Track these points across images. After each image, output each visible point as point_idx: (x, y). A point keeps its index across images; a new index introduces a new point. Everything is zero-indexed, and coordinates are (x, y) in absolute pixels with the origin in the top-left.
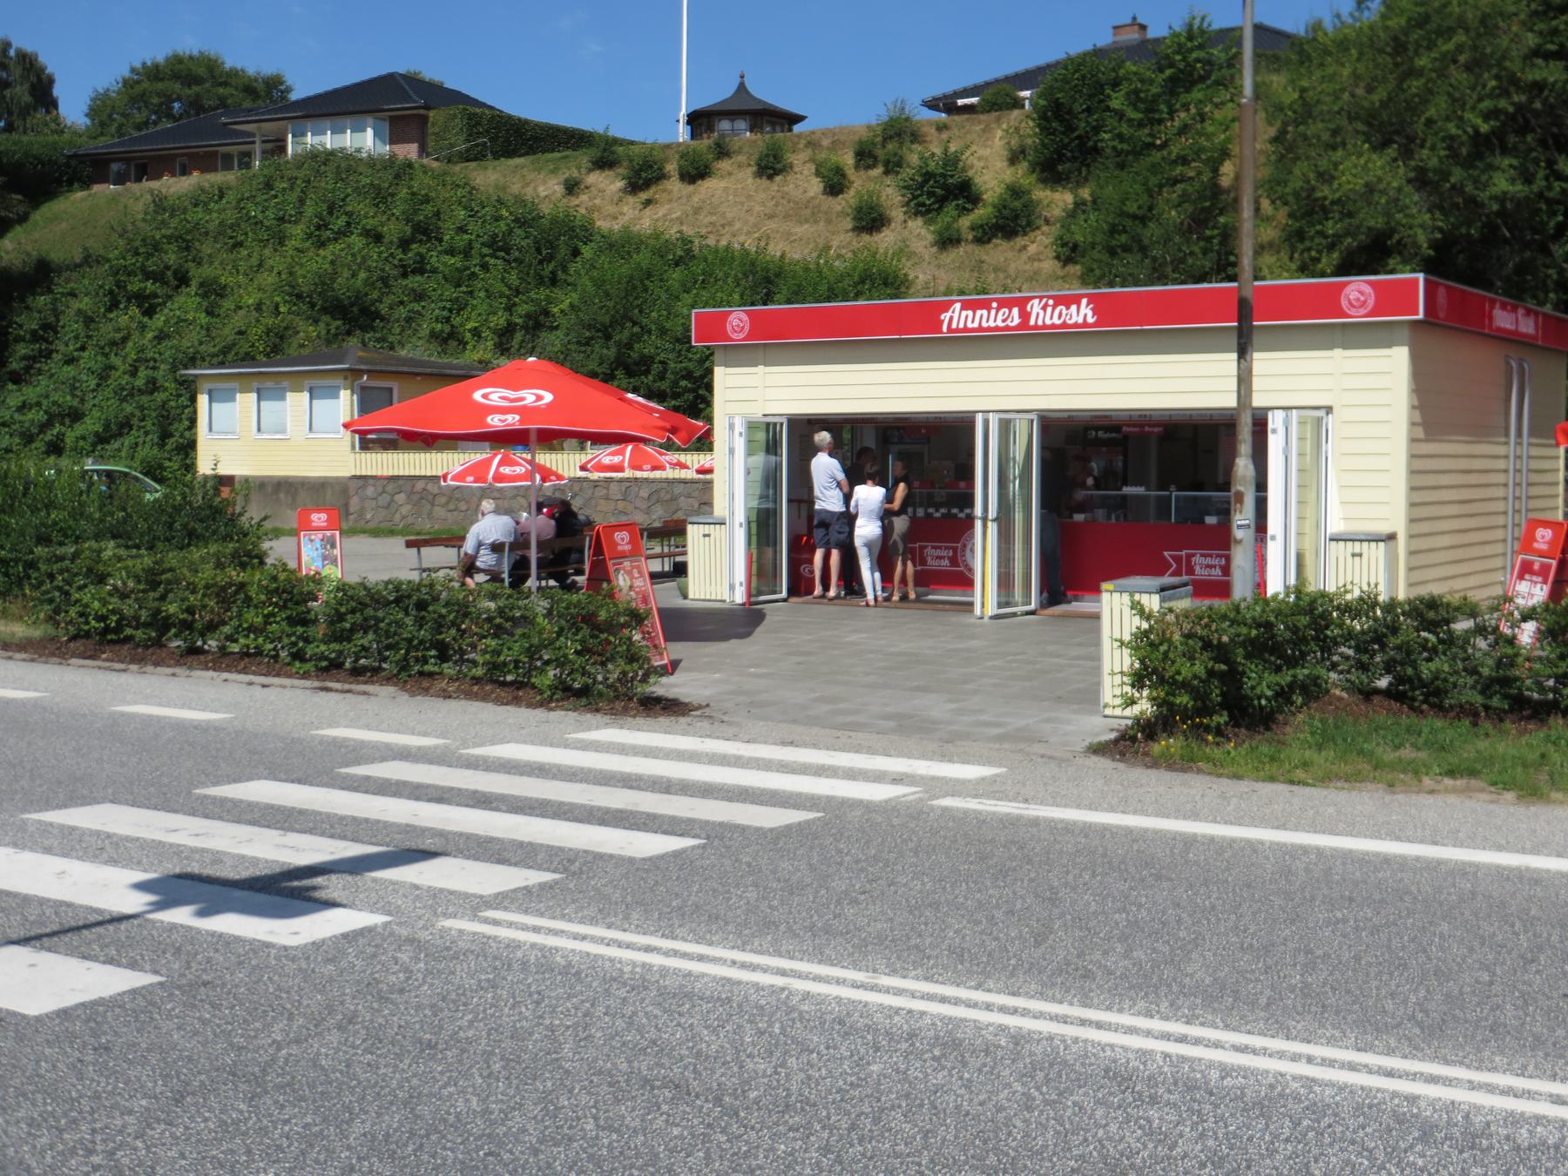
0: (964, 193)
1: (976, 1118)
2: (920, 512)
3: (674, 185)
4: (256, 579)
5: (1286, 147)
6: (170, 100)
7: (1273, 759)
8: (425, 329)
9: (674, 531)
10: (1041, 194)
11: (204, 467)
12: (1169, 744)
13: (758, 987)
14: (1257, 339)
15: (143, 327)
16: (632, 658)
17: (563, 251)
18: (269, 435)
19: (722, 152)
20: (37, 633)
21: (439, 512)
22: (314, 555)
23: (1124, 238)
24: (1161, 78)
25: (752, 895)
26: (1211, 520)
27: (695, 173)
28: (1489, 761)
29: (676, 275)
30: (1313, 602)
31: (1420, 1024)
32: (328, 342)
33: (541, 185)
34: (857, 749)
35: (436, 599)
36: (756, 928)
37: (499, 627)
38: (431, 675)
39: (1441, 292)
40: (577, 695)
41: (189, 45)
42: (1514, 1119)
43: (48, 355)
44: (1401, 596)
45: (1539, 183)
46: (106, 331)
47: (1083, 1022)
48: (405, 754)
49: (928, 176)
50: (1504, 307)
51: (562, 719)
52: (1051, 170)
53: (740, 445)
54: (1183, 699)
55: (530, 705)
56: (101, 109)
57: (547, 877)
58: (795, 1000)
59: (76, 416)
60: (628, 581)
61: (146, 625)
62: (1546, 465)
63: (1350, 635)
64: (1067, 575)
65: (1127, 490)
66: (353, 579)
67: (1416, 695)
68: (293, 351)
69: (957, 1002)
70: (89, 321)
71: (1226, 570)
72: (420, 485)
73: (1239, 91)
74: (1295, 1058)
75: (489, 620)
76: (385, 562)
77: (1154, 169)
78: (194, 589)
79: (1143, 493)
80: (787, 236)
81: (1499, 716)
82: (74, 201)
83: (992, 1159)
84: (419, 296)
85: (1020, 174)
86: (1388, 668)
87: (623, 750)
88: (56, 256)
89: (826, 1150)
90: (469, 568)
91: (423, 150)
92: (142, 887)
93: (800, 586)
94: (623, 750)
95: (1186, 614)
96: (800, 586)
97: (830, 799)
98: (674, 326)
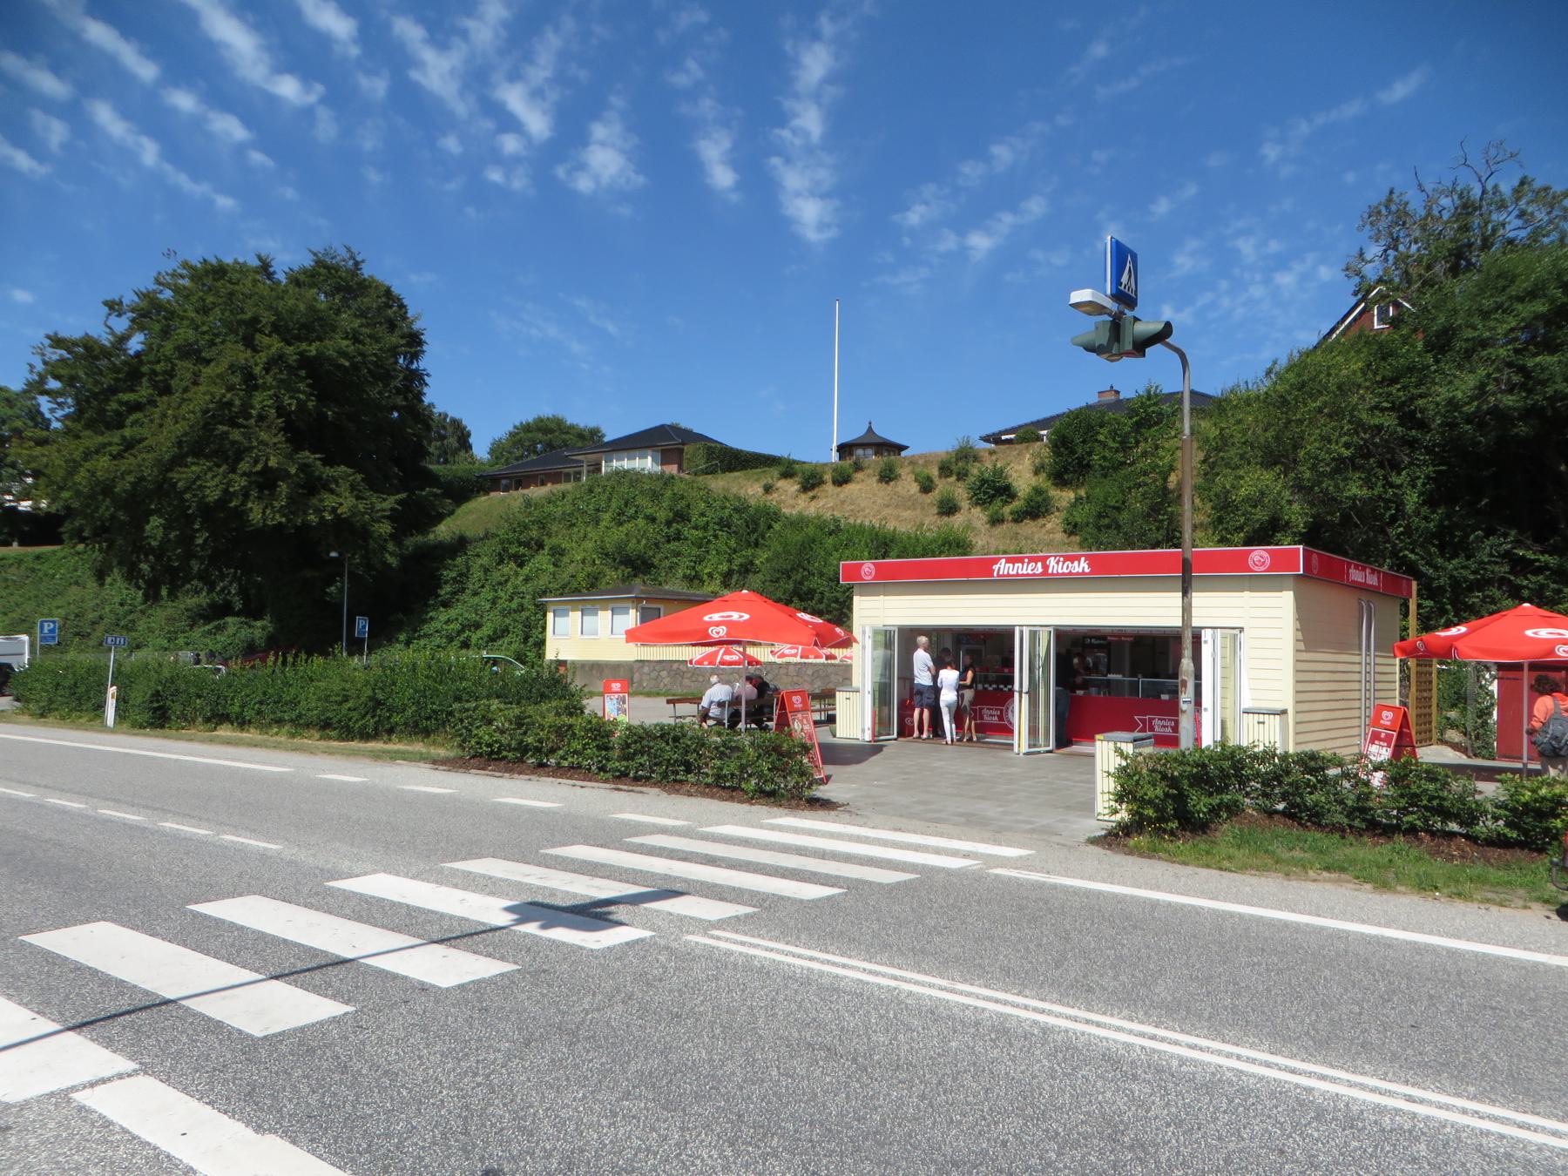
0: (1007, 492)
1: (1019, 1081)
2: (980, 687)
3: (829, 488)
4: (576, 722)
5: (1210, 468)
6: (534, 443)
7: (1208, 853)
8: (680, 573)
9: (828, 696)
10: (1054, 493)
11: (550, 655)
12: (1141, 840)
13: (880, 987)
14: (1194, 583)
15: (517, 574)
16: (802, 774)
17: (762, 526)
18: (585, 636)
19: (858, 467)
20: (452, 754)
21: (686, 682)
22: (616, 710)
23: (1107, 521)
24: (1130, 422)
25: (876, 926)
26: (1165, 697)
27: (842, 480)
28: (1353, 862)
29: (830, 541)
30: (1233, 753)
31: (1313, 1038)
32: (623, 581)
33: (749, 488)
34: (941, 835)
35: (684, 736)
36: (878, 948)
37: (722, 753)
38: (681, 782)
39: (1315, 556)
40: (768, 796)
41: (547, 411)
42: (1380, 1110)
43: (463, 590)
44: (1291, 751)
45: (1378, 490)
46: (496, 576)
47: (1088, 1022)
48: (664, 831)
49: (984, 481)
50: (1356, 567)
51: (760, 811)
52: (1060, 478)
53: (869, 643)
54: (1150, 812)
55: (740, 802)
56: (497, 450)
57: (749, 910)
58: (903, 996)
59: (478, 626)
60: (801, 726)
61: (515, 750)
62: (1388, 669)
63: (1258, 774)
64: (1073, 727)
65: (1110, 676)
66: (636, 723)
67: (1302, 815)
68: (602, 587)
69: (1006, 1003)
70: (486, 570)
71: (1176, 729)
72: (675, 666)
73: (1180, 432)
74: (1229, 1055)
75: (717, 748)
76: (653, 713)
77: (1126, 478)
78: (540, 728)
79: (1121, 679)
80: (897, 517)
81: (1360, 833)
82: (481, 503)
83: (1029, 1111)
84: (678, 554)
85: (1041, 481)
86: (1284, 797)
87: (796, 831)
88: (469, 534)
89: (923, 1097)
90: (705, 716)
91: (680, 469)
92: (509, 909)
93: (905, 731)
94: (796, 831)
95: (1151, 757)
96: (905, 731)
97: (924, 866)
98: (829, 571)
